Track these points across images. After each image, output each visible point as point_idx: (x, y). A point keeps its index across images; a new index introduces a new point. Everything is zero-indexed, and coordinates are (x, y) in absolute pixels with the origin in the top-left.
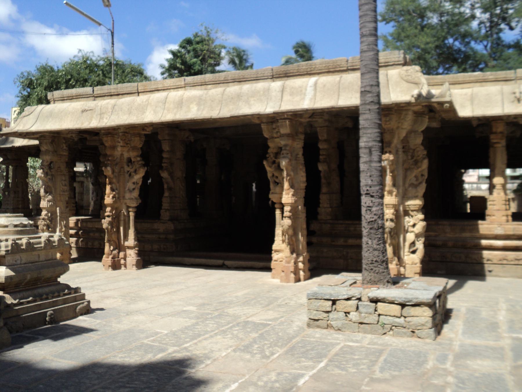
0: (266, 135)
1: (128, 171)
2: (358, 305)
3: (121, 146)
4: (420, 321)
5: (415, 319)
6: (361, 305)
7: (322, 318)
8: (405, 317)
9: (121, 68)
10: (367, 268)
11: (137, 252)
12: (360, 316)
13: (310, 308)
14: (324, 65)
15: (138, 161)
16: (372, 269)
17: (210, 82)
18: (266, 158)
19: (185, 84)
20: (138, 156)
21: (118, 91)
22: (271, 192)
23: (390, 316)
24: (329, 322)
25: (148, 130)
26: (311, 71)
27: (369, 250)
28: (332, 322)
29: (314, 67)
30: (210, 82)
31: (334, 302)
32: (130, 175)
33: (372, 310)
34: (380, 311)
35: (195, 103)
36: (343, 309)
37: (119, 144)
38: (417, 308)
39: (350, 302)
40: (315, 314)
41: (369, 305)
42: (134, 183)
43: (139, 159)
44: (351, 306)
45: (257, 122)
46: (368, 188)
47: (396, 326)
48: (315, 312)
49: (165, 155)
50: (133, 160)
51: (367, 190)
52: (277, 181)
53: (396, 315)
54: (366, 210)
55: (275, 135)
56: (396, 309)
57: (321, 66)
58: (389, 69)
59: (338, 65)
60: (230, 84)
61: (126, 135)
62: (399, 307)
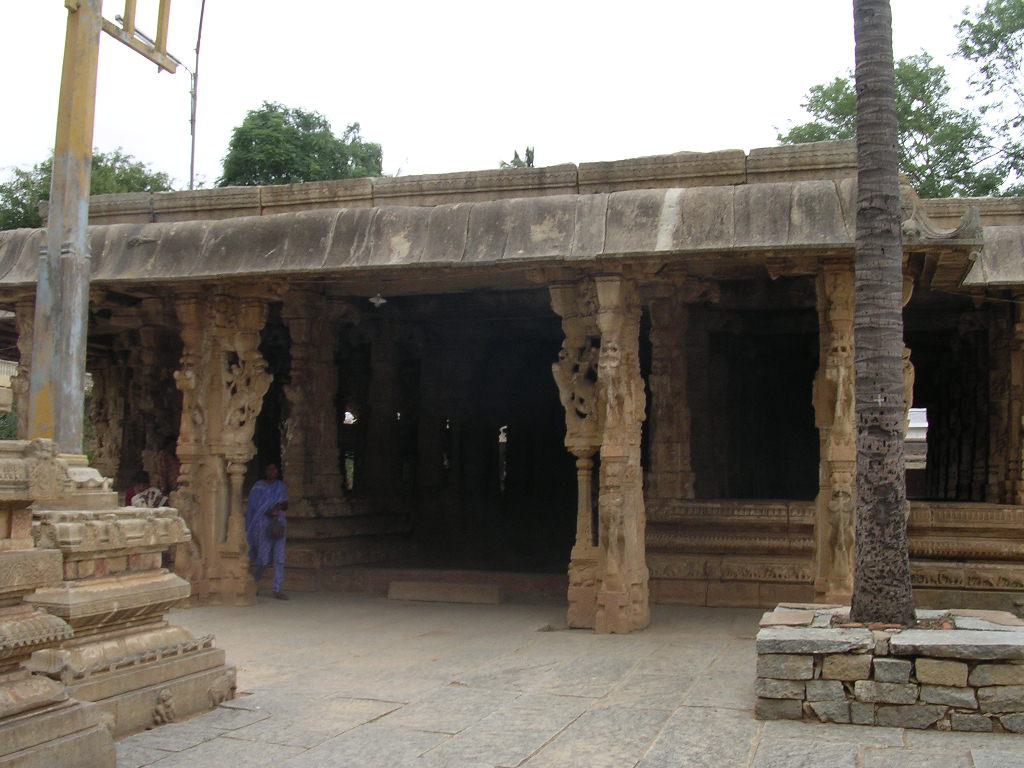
0: (558, 308)
1: (229, 384)
2: (872, 664)
3: (217, 326)
4: (1011, 696)
5: (1000, 690)
6: (880, 664)
7: (791, 696)
8: (976, 688)
9: (245, 147)
10: (869, 589)
11: (245, 565)
12: (878, 688)
13: (763, 674)
14: (694, 164)
15: (256, 361)
16: (880, 590)
17: (131, 210)
18: (556, 359)
19: (372, 193)
20: (252, 350)
21: (213, 202)
22: (568, 433)
23: (944, 686)
24: (806, 704)
25: (279, 291)
26: (664, 175)
27: (874, 549)
28: (812, 704)
29: (670, 166)
30: (131, 210)
31: (819, 659)
32: (234, 391)
33: (903, 675)
34: (920, 676)
35: (403, 234)
36: (839, 674)
37: (213, 322)
38: (1002, 668)
39: (853, 661)
40: (776, 688)
41: (896, 664)
42: (242, 410)
43: (257, 356)
44: (858, 668)
45: (539, 279)
46: (877, 415)
47: (956, 708)
48: (775, 683)
49: (295, 352)
50: (241, 357)
51: (876, 419)
52: (582, 409)
53: (958, 684)
54: (870, 462)
55: (583, 310)
56: (958, 673)
57: (687, 164)
58: (505, 197)
59: (726, 165)
60: (479, 195)
61: (229, 300)
62: (964, 667)
